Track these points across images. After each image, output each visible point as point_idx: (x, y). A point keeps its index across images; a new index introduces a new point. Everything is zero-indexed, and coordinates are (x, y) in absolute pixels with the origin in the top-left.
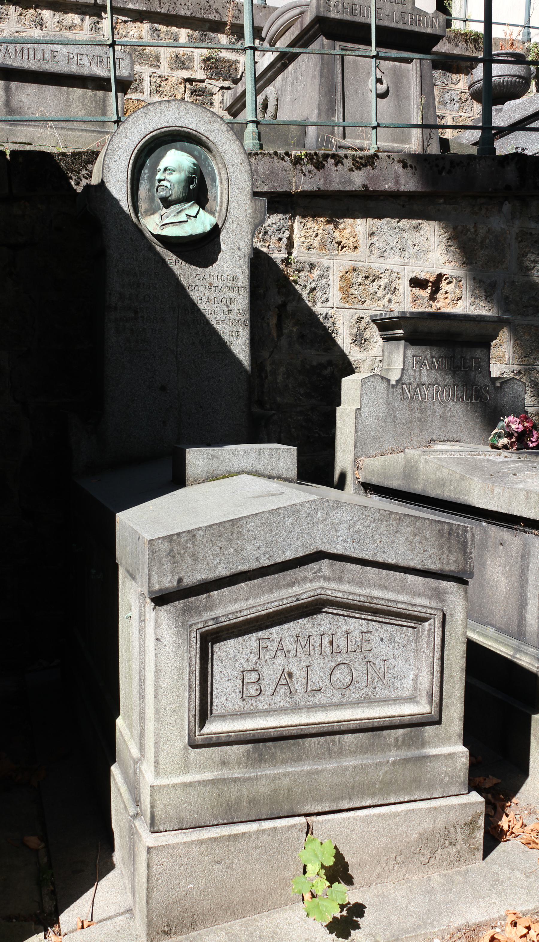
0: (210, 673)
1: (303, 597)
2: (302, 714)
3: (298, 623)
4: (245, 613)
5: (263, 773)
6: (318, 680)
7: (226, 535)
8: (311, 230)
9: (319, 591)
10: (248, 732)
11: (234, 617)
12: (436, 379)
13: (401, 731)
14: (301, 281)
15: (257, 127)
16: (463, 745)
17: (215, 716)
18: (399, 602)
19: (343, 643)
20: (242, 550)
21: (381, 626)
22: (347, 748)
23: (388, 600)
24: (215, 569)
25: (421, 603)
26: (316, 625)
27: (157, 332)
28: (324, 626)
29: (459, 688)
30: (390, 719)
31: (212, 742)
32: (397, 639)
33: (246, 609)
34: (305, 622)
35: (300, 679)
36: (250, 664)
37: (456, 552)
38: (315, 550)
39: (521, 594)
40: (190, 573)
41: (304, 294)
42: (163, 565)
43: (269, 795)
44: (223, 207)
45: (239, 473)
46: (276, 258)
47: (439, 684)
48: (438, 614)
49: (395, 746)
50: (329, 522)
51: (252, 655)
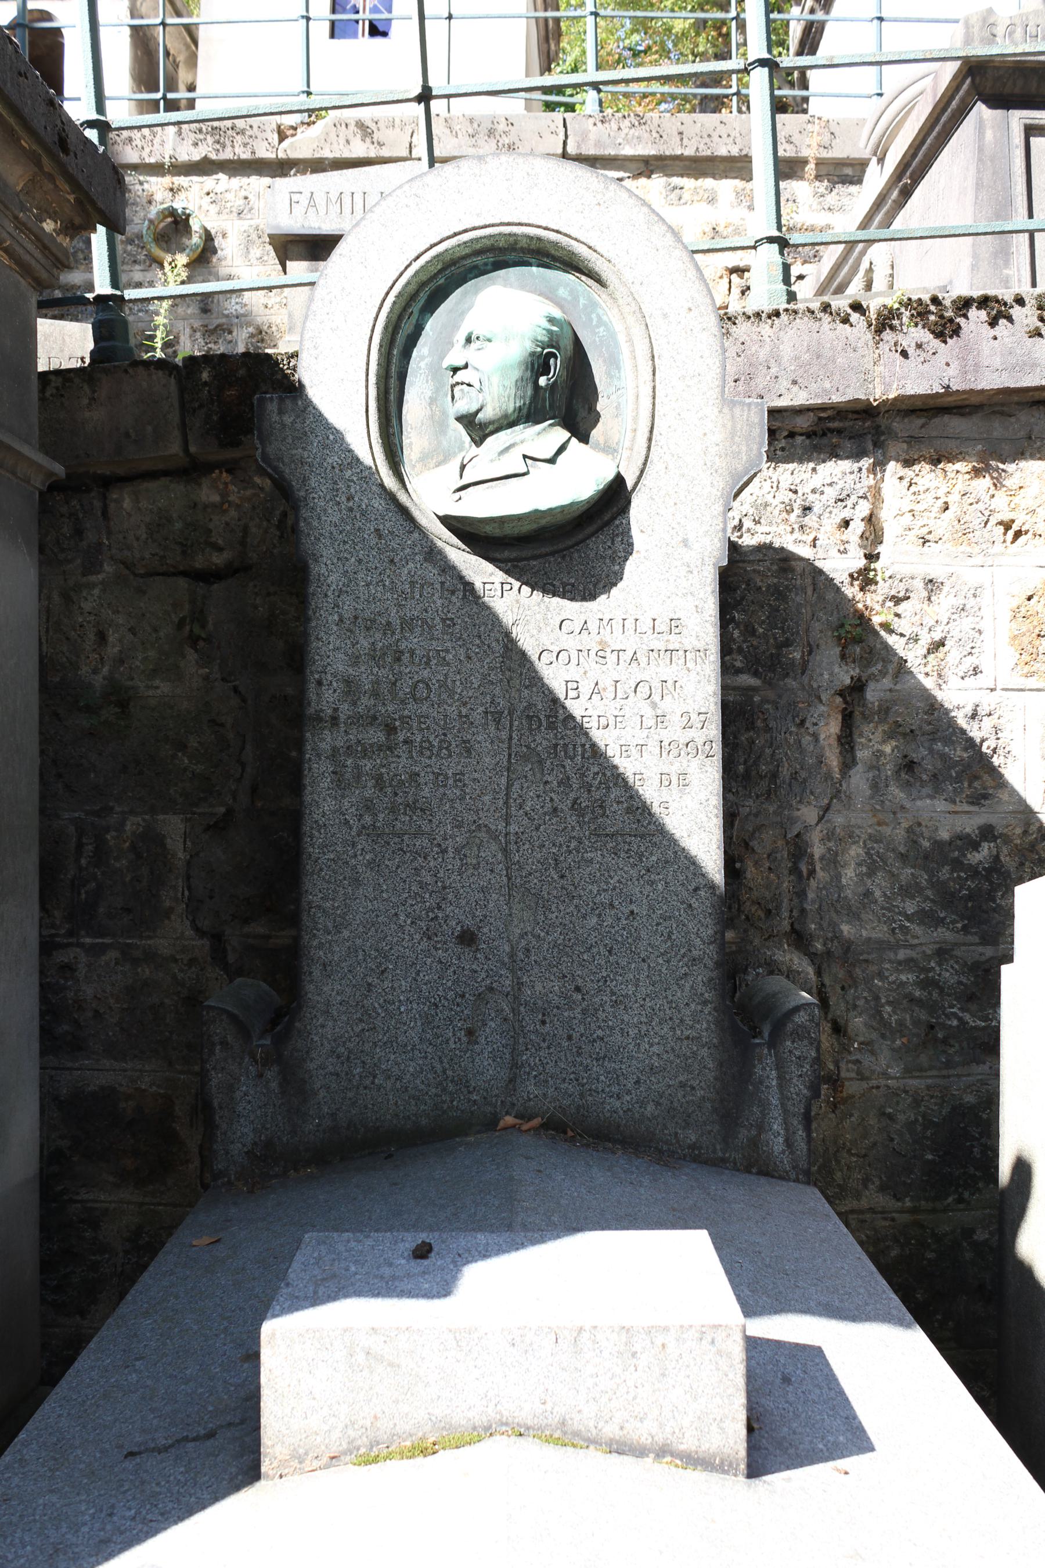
8: (929, 497)
14: (902, 626)
15: (781, 253)
27: (451, 782)
41: (913, 656)
44: (639, 433)
45: (488, 1431)
46: (835, 570)
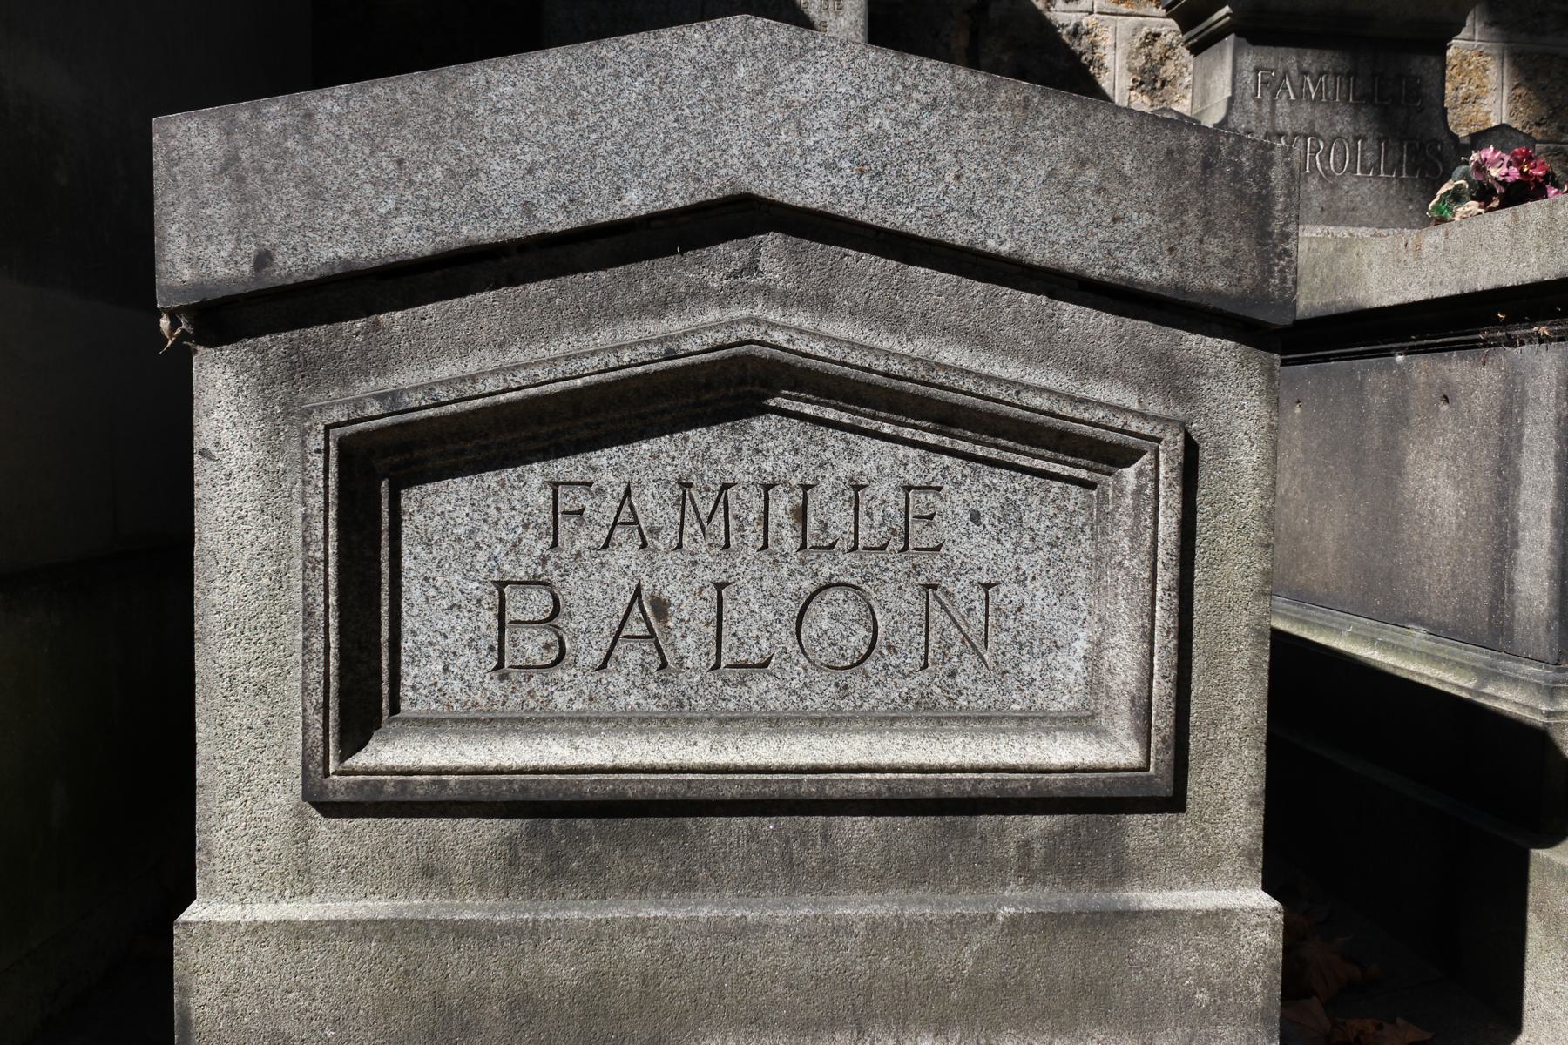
0: (385, 579)
1: (688, 345)
2: (695, 737)
3: (686, 439)
4: (491, 384)
5: (560, 914)
6: (755, 633)
7: (420, 120)
9: (743, 332)
10: (504, 777)
11: (453, 396)
12: (1312, 123)
13: (1040, 823)
16: (1265, 889)
17: (406, 720)
18: (1028, 387)
19: (840, 519)
20: (474, 173)
21: (974, 470)
22: (852, 860)
23: (990, 378)
24: (380, 229)
25: (1111, 401)
26: (745, 452)
28: (776, 457)
29: (1249, 695)
30: (999, 776)
31: (381, 798)
32: (1029, 519)
33: (492, 372)
34: (708, 438)
35: (692, 625)
36: (525, 561)
37: (1230, 228)
38: (728, 191)
39: (1498, 520)
40: (296, 239)
42: (205, 205)
43: (577, 990)
47: (1173, 674)
48: (1168, 437)
49: (1021, 869)
50: (777, 100)
51: (530, 535)
